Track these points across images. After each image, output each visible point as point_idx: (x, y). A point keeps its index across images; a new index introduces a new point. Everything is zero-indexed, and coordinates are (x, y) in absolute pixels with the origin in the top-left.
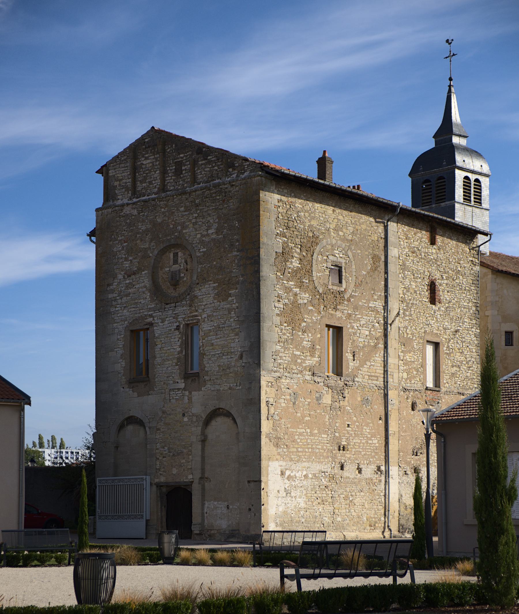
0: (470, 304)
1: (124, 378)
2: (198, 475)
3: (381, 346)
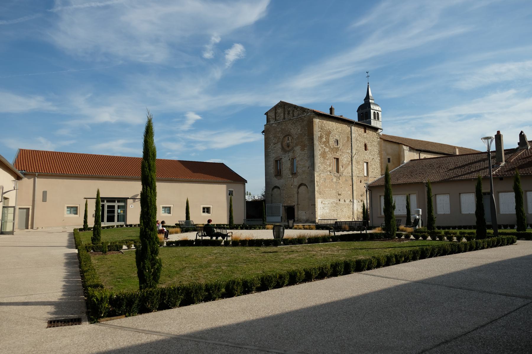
2: (296, 203)
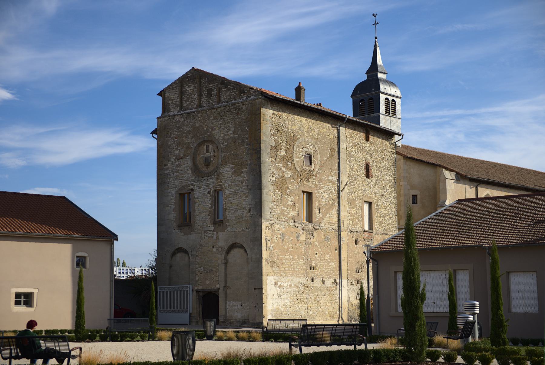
0: (391, 178)
2: (222, 284)
3: (336, 204)
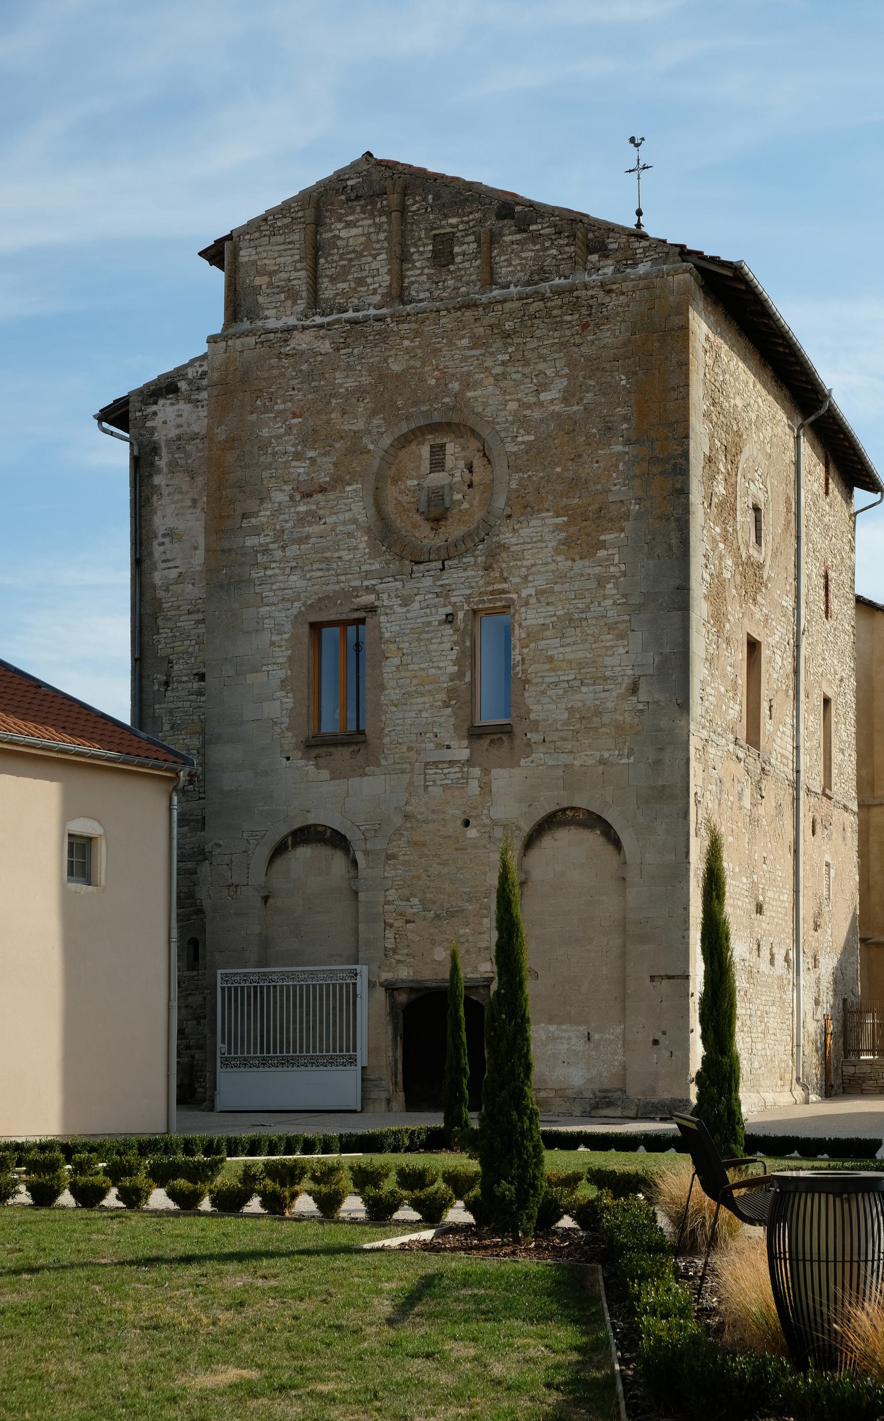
1: (290, 734)
